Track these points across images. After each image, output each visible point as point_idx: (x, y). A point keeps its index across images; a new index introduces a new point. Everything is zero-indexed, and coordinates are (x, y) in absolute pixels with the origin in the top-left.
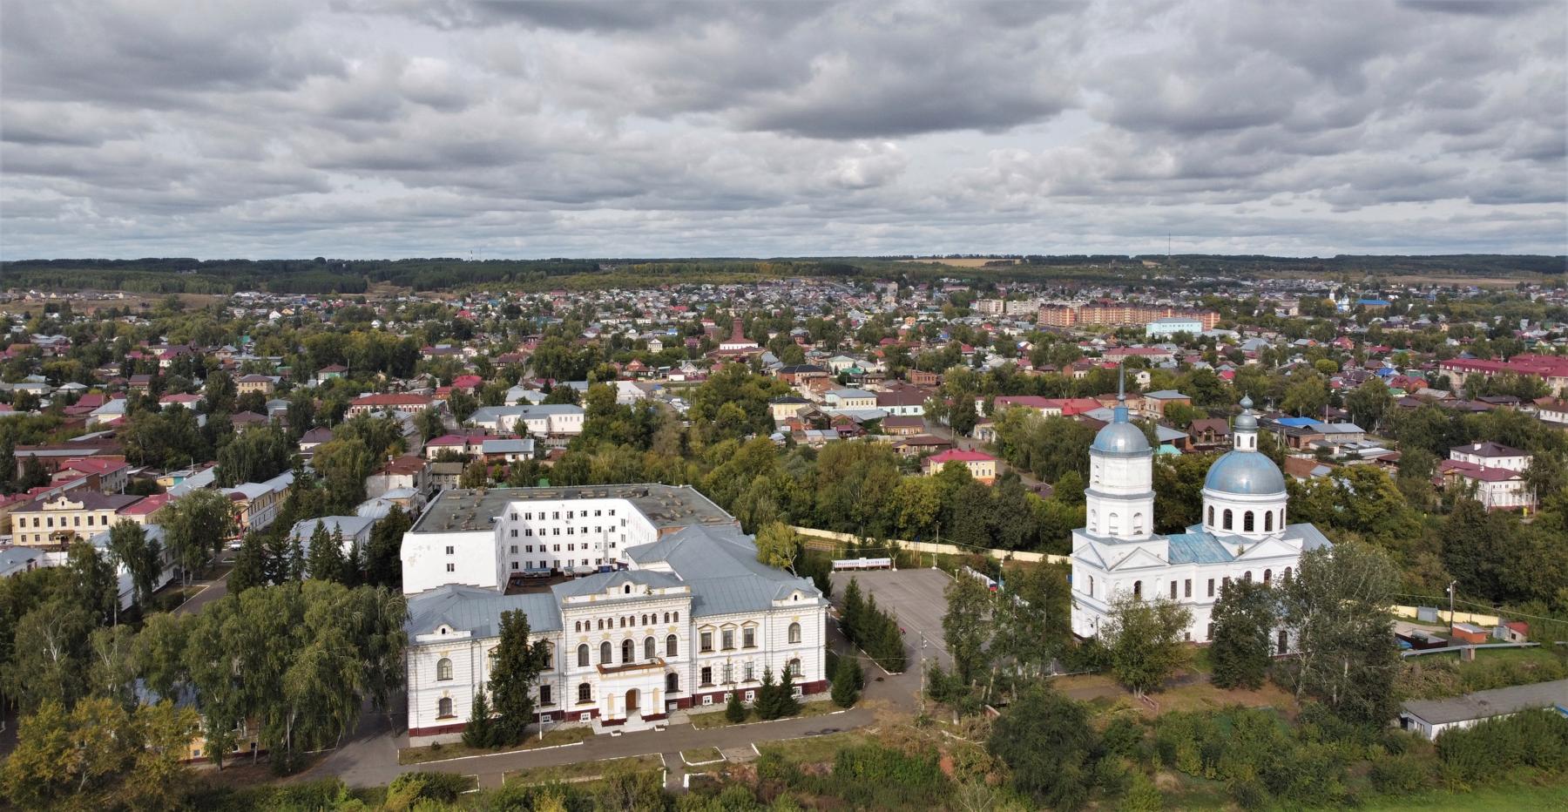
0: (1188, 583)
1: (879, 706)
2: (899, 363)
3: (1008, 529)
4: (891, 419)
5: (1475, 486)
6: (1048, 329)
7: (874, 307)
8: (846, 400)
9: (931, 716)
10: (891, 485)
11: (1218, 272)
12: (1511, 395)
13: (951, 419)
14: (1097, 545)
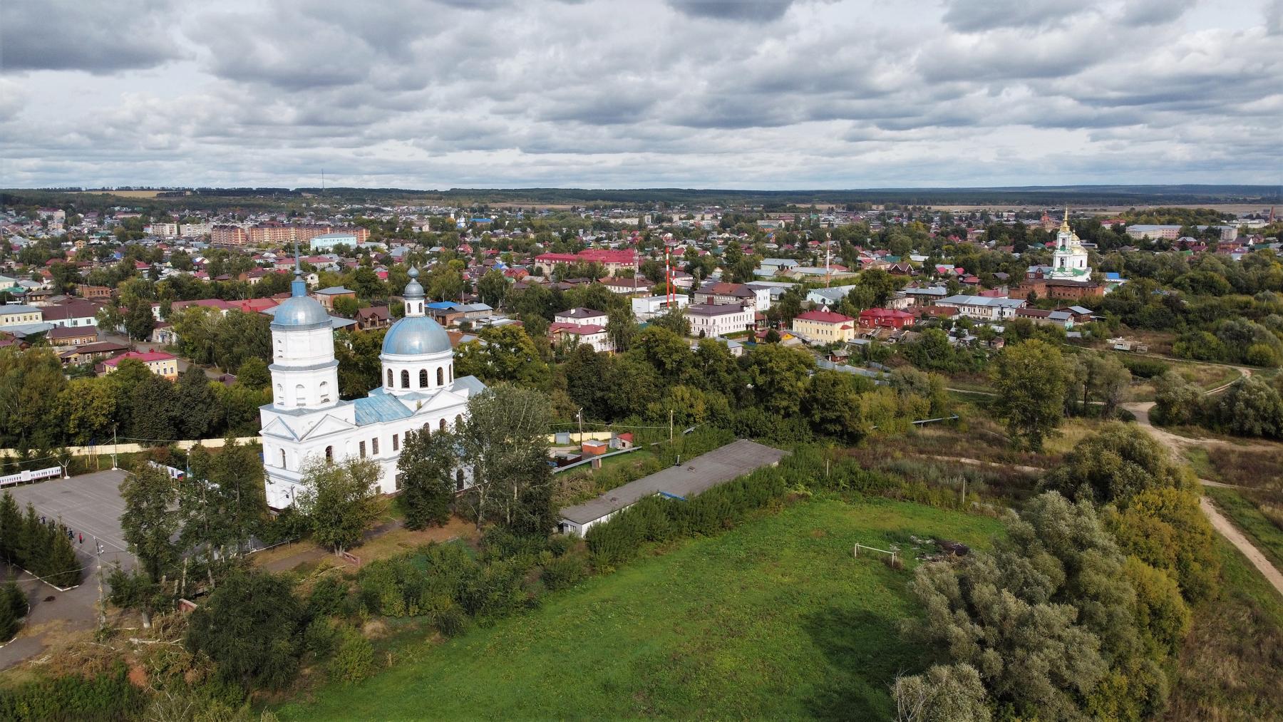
0: (375, 441)
1: (50, 629)
2: (67, 280)
3: (192, 419)
4: (59, 332)
8: (5, 317)
9: (116, 625)
10: (53, 390)
11: (364, 201)
12: (585, 277)
13: (127, 326)
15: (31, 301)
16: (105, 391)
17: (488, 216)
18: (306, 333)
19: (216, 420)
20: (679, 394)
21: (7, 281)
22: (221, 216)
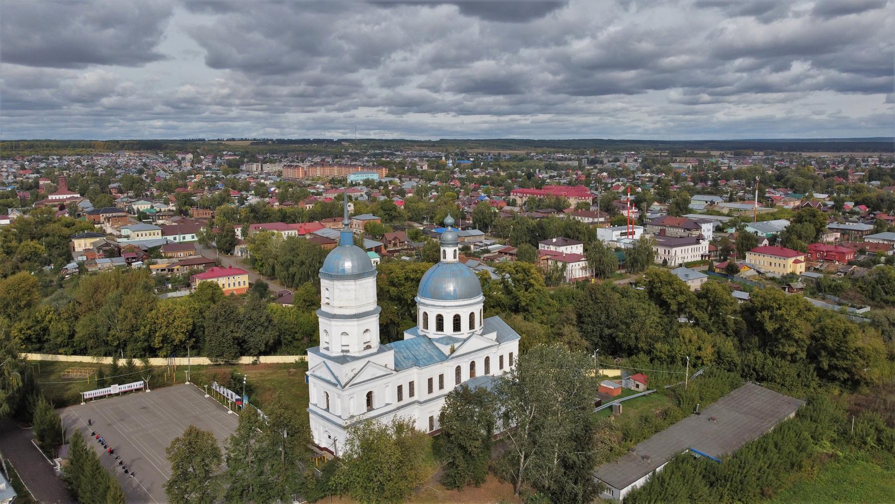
0: (411, 384)
2: (185, 204)
3: (252, 339)
4: (169, 246)
5: (564, 267)
6: (289, 180)
7: (175, 169)
8: (137, 233)
10: (145, 310)
14: (330, 363)
15: (159, 219)
16: (184, 312)
17: (468, 159)
18: (352, 283)
19: (271, 341)
20: (687, 336)
21: (145, 204)
22: (290, 158)
